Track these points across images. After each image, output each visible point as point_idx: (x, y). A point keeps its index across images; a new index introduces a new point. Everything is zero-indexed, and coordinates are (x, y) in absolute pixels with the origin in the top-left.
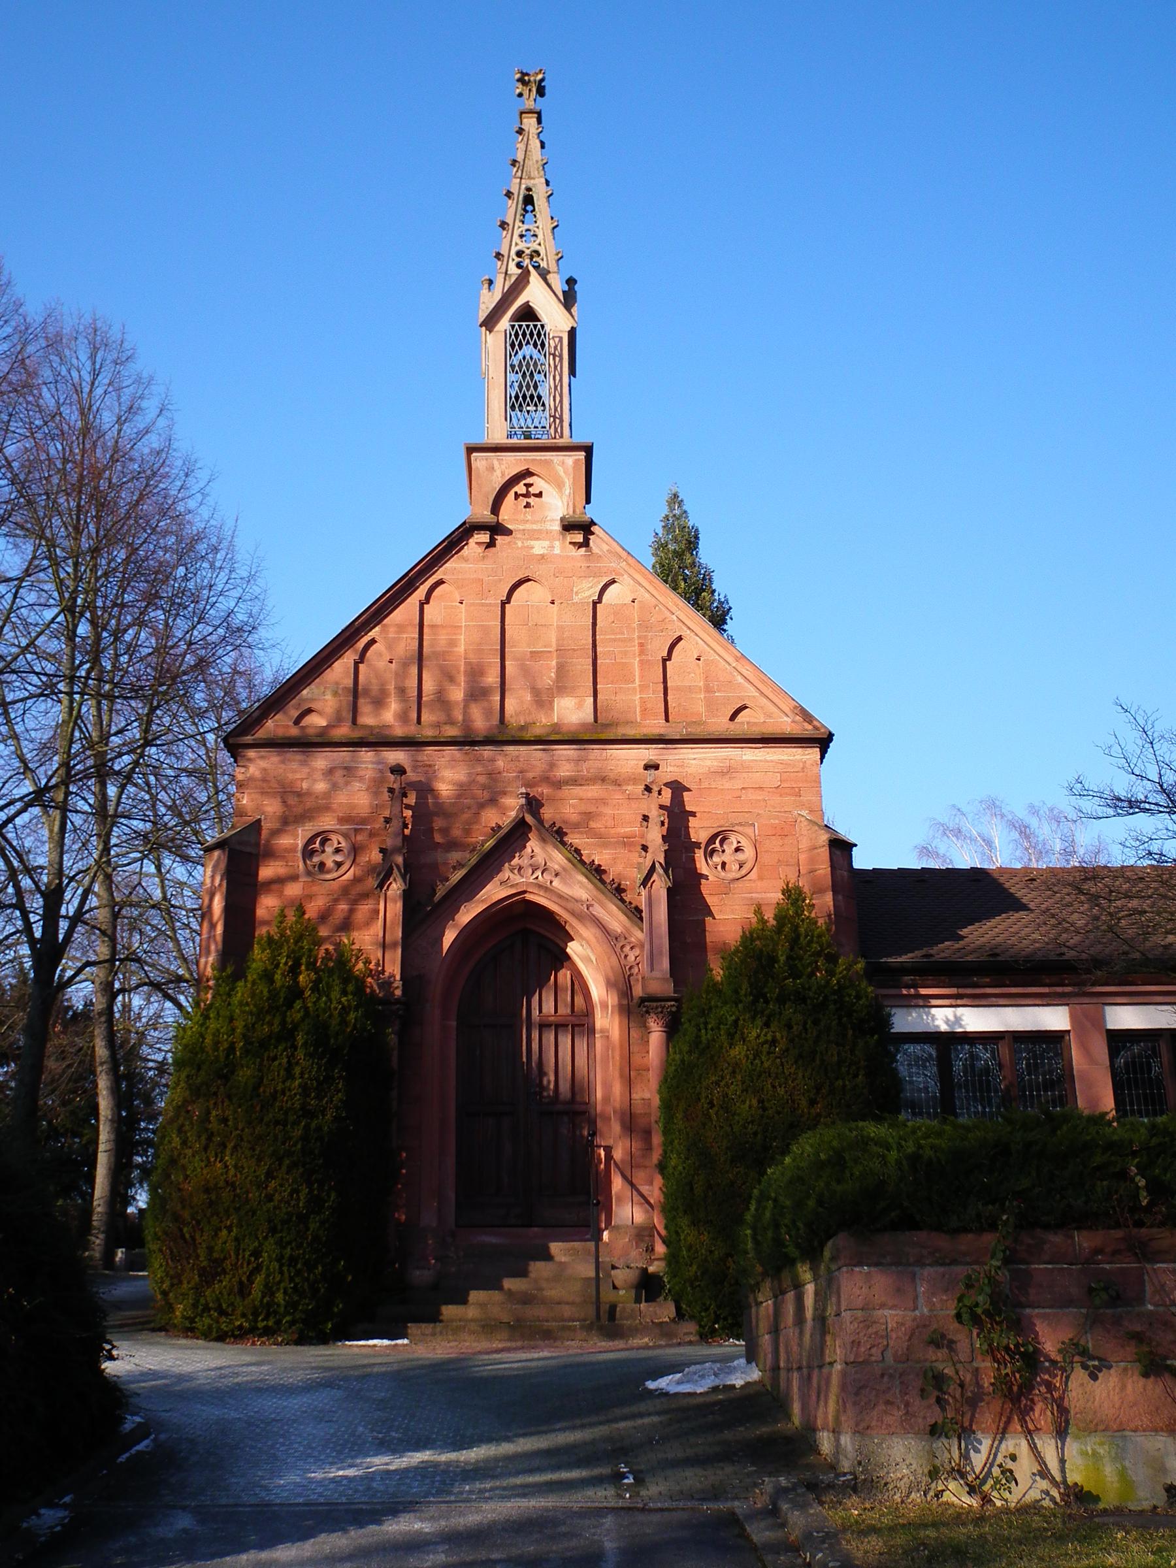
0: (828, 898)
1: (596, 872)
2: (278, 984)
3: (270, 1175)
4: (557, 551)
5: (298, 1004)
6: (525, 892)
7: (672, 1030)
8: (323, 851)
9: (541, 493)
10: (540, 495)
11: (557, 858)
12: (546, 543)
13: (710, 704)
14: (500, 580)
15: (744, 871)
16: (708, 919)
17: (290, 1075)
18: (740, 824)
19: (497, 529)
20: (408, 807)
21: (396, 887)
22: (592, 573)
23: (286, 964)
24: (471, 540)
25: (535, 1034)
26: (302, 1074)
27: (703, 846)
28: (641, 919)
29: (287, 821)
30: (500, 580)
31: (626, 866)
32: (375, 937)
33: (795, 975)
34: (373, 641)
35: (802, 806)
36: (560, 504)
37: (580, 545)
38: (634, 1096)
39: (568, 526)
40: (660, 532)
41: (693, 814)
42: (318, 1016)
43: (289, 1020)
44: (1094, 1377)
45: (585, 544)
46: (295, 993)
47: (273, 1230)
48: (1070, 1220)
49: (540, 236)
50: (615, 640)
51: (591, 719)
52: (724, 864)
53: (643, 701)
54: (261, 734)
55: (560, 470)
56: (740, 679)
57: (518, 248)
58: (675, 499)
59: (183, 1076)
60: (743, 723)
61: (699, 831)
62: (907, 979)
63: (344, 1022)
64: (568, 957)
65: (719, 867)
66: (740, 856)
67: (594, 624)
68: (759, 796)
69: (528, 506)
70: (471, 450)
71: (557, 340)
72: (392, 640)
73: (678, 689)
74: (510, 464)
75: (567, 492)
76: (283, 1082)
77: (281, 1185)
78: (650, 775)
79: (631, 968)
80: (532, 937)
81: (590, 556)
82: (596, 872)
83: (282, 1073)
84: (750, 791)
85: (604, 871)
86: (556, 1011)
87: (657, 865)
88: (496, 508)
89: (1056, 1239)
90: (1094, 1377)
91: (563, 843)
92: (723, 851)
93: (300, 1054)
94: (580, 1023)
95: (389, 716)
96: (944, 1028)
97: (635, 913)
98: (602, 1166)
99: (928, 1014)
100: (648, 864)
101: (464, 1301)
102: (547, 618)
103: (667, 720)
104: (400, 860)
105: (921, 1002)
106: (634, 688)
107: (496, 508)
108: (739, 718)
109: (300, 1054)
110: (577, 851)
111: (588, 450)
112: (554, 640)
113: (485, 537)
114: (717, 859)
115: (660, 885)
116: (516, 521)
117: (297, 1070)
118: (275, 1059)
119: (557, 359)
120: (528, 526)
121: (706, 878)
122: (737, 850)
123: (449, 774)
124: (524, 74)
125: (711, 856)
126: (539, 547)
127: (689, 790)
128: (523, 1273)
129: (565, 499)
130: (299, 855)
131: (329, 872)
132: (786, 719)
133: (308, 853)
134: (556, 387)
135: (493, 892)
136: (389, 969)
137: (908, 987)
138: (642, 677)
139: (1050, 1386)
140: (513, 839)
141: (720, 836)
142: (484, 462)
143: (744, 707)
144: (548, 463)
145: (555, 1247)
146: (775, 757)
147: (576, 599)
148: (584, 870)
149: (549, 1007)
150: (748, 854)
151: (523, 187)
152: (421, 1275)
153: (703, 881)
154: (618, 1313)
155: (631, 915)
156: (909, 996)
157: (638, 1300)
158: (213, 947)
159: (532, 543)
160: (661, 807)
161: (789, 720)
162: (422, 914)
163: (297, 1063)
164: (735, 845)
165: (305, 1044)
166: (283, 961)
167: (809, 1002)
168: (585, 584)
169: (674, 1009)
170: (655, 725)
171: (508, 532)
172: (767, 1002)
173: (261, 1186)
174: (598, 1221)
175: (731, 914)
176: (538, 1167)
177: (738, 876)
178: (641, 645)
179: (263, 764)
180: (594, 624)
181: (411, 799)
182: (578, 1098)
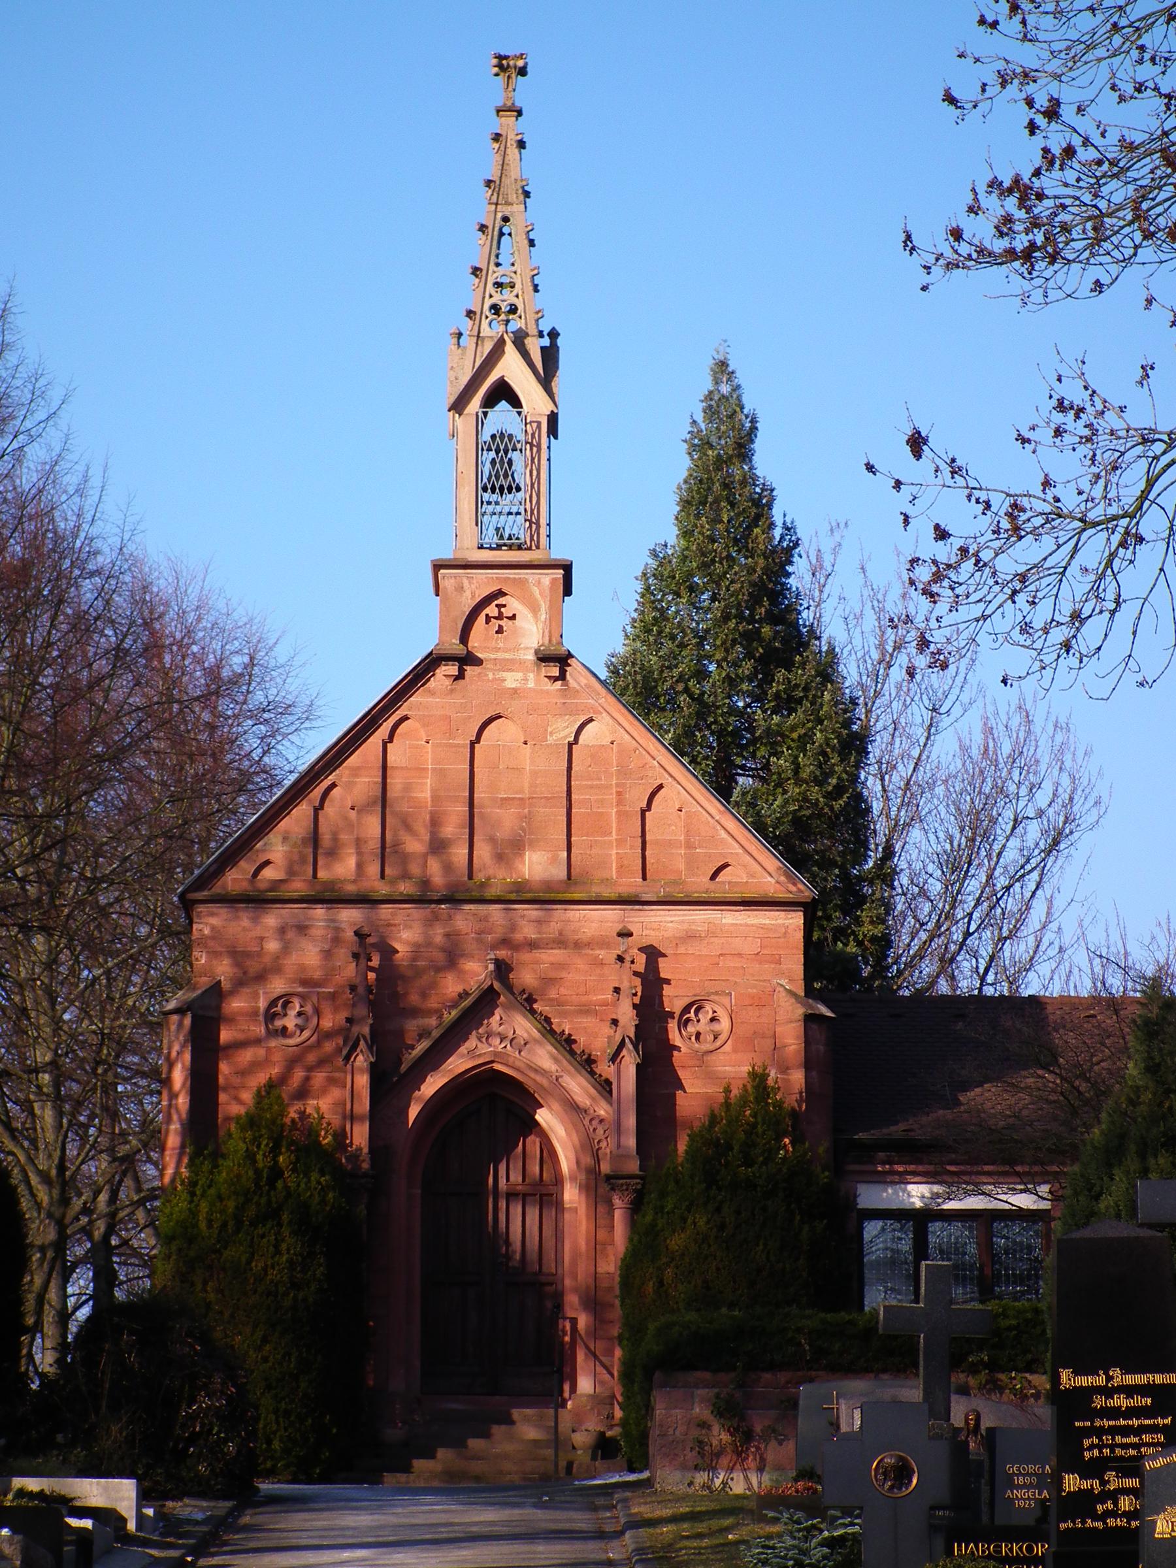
0: (798, 1077)
1: (566, 1043)
2: (260, 1165)
3: (265, 1340)
4: (531, 685)
5: (279, 1184)
6: (492, 1062)
7: (636, 1208)
8: (285, 1015)
9: (514, 615)
10: (513, 617)
11: (523, 1026)
12: (519, 675)
13: (691, 861)
14: (470, 717)
15: (718, 1043)
16: (679, 1093)
17: (278, 1252)
18: (716, 993)
19: (468, 660)
20: (372, 969)
21: (361, 1060)
22: (567, 710)
23: (267, 1145)
24: (437, 671)
25: (502, 1204)
26: (288, 1250)
27: (677, 1016)
28: (610, 1092)
29: (240, 983)
30: (470, 717)
31: (596, 1037)
32: (338, 1101)
33: (748, 1162)
34: (334, 785)
35: (782, 974)
36: (535, 629)
37: (556, 679)
38: (599, 1270)
39: (544, 658)
40: (699, 417)
41: (668, 982)
42: (299, 1195)
43: (274, 1199)
44: (780, 1444)
45: (562, 677)
46: (276, 1173)
47: (269, 1387)
48: (772, 1367)
49: (518, 286)
50: (591, 787)
51: (563, 874)
52: (698, 1035)
53: (620, 857)
54: (217, 889)
55: (536, 591)
56: (723, 834)
57: (493, 301)
58: (722, 368)
59: (174, 1248)
60: (724, 883)
61: (674, 999)
62: (882, 1155)
63: (323, 1202)
64: (537, 1124)
65: (693, 1038)
66: (716, 1027)
67: (570, 768)
68: (736, 963)
69: (500, 630)
70: (438, 566)
71: (535, 425)
72: (355, 780)
73: (657, 842)
74: (478, 584)
75: (543, 617)
76: (272, 1257)
77: (275, 1349)
78: (622, 945)
79: (599, 1142)
80: (498, 1108)
81: (566, 691)
82: (566, 1043)
83: (271, 1249)
84: (729, 957)
85: (575, 1041)
86: (524, 1180)
87: (627, 1040)
88: (464, 638)
89: (767, 1376)
90: (780, 1444)
91: (533, 1012)
92: (698, 1021)
93: (286, 1231)
94: (544, 1194)
95: (344, 868)
96: (918, 1204)
97: (605, 1087)
98: (567, 1339)
99: (904, 1190)
100: (618, 1038)
101: (432, 1456)
102: (519, 759)
103: (644, 878)
104: (366, 1030)
105: (897, 1178)
106: (610, 841)
107: (464, 638)
108: (721, 878)
109: (286, 1231)
110: (548, 1020)
111: (567, 568)
112: (526, 785)
113: (453, 669)
114: (691, 1029)
115: (630, 1062)
116: (485, 649)
117: (284, 1246)
118: (263, 1236)
119: (535, 449)
120: (500, 655)
121: (678, 1049)
122: (713, 1020)
123: (407, 933)
124: (500, 58)
125: (685, 1026)
126: (512, 680)
127: (664, 955)
128: (487, 1435)
129: (541, 626)
130: (261, 1018)
131: (291, 1036)
132: (769, 879)
133: (270, 1016)
134: (532, 485)
135: (457, 1064)
136: (356, 1142)
137: (883, 1163)
138: (619, 830)
139: (758, 1448)
140: (481, 1006)
141: (697, 1005)
142: (452, 581)
143: (726, 865)
144: (522, 582)
145: (516, 1413)
146: (755, 921)
147: (551, 740)
148: (553, 1041)
149: (515, 1177)
150: (724, 1024)
151: (499, 215)
152: (394, 1434)
153: (675, 1053)
154: (575, 1470)
155: (600, 1088)
156: (884, 1173)
157: (594, 1458)
158: (175, 1117)
159: (505, 674)
160: (636, 974)
161: (773, 881)
162: (390, 1083)
163: (283, 1240)
164: (710, 1015)
165: (290, 1222)
166: (265, 1142)
167: (759, 1189)
168: (561, 723)
169: (639, 1187)
170: (631, 883)
171: (478, 662)
172: (719, 1189)
173: (259, 1349)
174: (561, 1391)
175: (696, 1093)
176: (500, 1335)
177: (712, 1048)
178: (619, 793)
179: (214, 921)
180: (570, 768)
181: (375, 962)
182: (545, 1269)
